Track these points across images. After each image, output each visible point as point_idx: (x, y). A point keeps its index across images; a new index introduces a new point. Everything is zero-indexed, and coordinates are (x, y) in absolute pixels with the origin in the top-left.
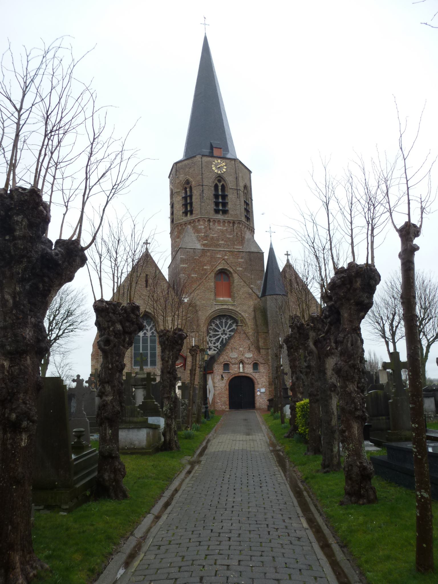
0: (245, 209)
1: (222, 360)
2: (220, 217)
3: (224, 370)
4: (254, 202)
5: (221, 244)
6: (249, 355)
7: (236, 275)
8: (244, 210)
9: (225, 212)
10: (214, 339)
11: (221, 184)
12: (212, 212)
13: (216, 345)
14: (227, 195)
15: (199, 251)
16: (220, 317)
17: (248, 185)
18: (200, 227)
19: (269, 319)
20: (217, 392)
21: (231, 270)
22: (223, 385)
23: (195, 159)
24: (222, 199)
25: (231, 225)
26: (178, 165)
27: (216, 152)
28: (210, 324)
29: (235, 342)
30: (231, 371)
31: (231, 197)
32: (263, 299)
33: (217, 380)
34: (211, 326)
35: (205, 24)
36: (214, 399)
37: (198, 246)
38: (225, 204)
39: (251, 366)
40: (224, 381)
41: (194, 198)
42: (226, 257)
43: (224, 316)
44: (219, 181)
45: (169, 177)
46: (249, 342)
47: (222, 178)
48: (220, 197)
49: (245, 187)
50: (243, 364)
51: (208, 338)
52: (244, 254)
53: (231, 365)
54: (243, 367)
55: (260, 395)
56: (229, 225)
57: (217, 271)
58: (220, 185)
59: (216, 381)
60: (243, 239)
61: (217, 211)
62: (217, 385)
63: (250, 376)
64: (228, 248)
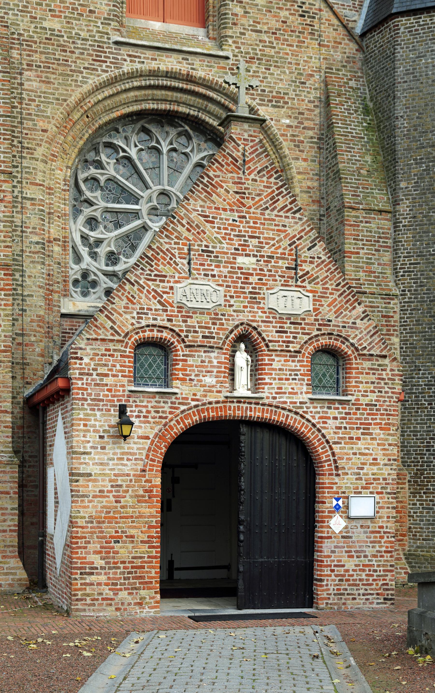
1: (127, 321)
6: (292, 301)
10: (109, 236)
13: (119, 268)
19: (401, 144)
20: (90, 509)
22: (130, 467)
30: (178, 388)
33: (92, 437)
34: (99, 165)
39: (300, 365)
50: (253, 350)
51: (77, 228)
53: (181, 351)
54: (256, 371)
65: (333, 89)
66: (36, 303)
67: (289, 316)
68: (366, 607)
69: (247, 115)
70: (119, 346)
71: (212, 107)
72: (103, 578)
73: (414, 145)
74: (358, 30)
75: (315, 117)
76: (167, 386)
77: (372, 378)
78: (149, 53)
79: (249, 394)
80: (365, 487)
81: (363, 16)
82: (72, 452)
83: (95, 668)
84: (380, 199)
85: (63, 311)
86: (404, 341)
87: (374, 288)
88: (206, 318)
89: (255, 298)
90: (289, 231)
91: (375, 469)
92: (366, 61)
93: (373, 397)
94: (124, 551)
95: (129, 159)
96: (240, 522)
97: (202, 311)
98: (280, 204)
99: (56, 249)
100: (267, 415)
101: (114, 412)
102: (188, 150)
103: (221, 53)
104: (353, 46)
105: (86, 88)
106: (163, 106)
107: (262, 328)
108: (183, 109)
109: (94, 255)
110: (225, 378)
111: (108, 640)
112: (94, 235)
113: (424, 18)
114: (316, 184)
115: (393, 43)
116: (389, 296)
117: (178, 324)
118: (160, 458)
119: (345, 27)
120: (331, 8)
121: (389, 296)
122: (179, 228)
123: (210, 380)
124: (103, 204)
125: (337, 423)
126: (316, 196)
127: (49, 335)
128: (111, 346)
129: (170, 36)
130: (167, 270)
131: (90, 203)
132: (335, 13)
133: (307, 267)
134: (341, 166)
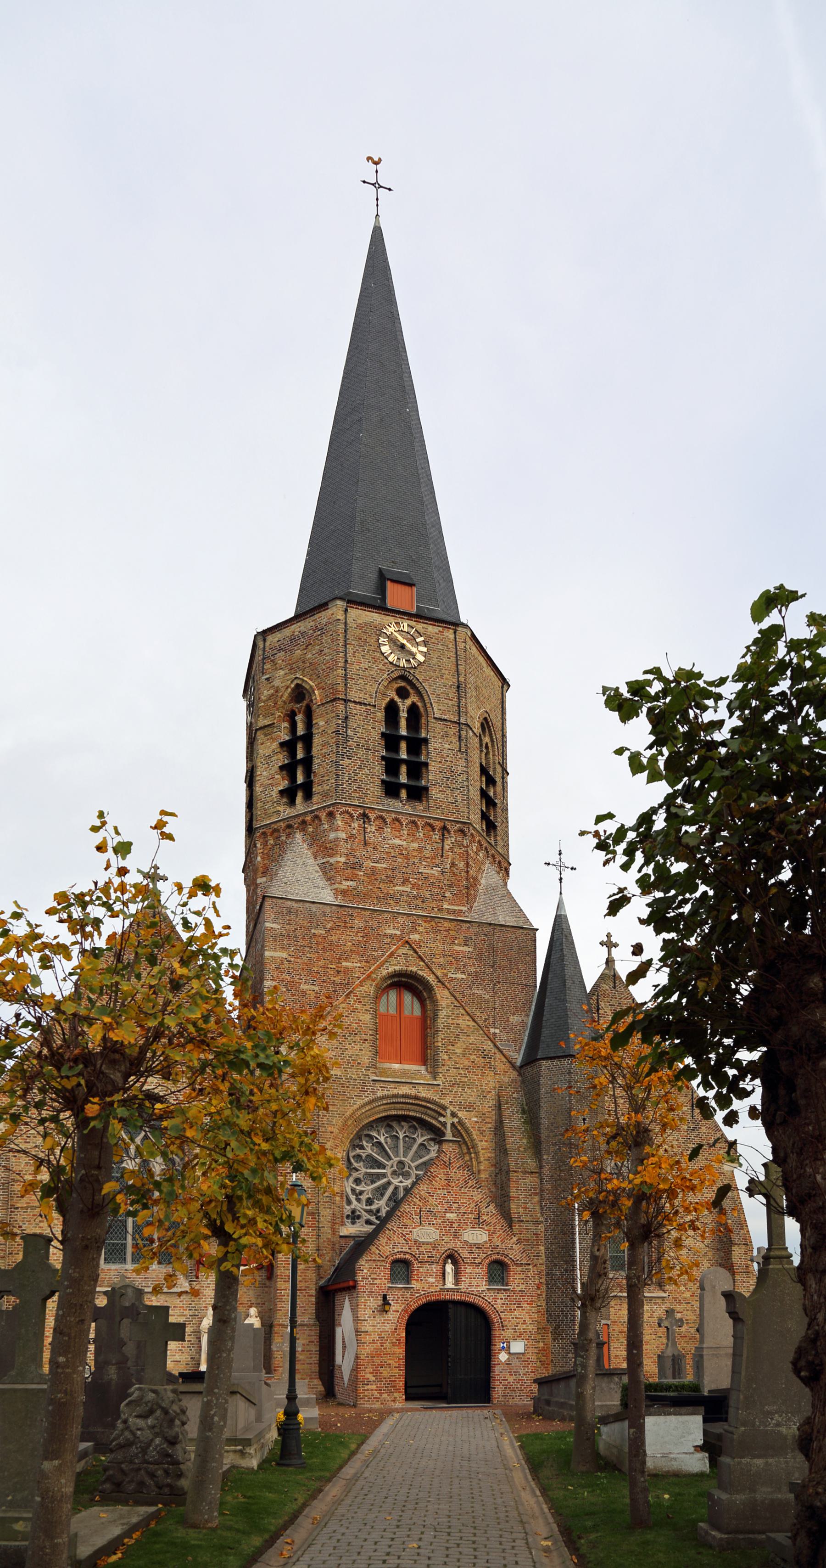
0: (484, 794)
1: (387, 1250)
2: (401, 806)
3: (393, 1278)
4: (511, 781)
5: (402, 894)
6: (477, 1236)
7: (446, 992)
8: (478, 769)
9: (418, 794)
10: (368, 1189)
11: (408, 702)
12: (375, 790)
13: (374, 1207)
14: (426, 741)
15: (328, 909)
16: (388, 1121)
17: (495, 720)
18: (332, 836)
19: (544, 1134)
20: (367, 1350)
21: (431, 979)
22: (388, 1327)
23: (323, 617)
24: (409, 752)
25: (436, 836)
26: (270, 638)
27: (396, 595)
28: (356, 1144)
29: (433, 1193)
30: (415, 1284)
31: (440, 747)
32: (529, 1070)
33: (368, 1312)
35: (377, 185)
36: (355, 1370)
37: (327, 896)
38: (417, 769)
39: (482, 1271)
40: (392, 1316)
41: (317, 741)
42: (415, 937)
43: (401, 1119)
44: (402, 693)
45: (244, 696)
46: (477, 1196)
47: (410, 683)
48: (403, 745)
49: (486, 725)
50: (455, 1263)
51: (349, 1185)
52: (474, 929)
54: (457, 1274)
55: (508, 1363)
56: (430, 837)
57: (385, 979)
58: (403, 706)
59: (365, 1313)
60: (472, 884)
61: (391, 790)
62: (370, 1329)
63: (478, 1301)
64: (422, 909)
65: (503, 1100)
66: (327, 1230)
67: (475, 1244)
68: (521, 1403)
69: (451, 1138)
70: (383, 1264)
71: (429, 1112)
72: (374, 1387)
73: (551, 1134)
74: (518, 1064)
75: (492, 1117)
76: (408, 1283)
77: (523, 1276)
78: (392, 1085)
79: (453, 1287)
80: (519, 1336)
81: (521, 1055)
82: (356, 1320)
83: (380, 1424)
84: (532, 1164)
85: (341, 1234)
86: (547, 1249)
87: (528, 1218)
88: (429, 1247)
89: (456, 1235)
90: (475, 1198)
91: (524, 1326)
92: (523, 1082)
93: (523, 1287)
94: (385, 1372)
95: (380, 1143)
96: (449, 1356)
97: (427, 1243)
98: (470, 1184)
99: (338, 1198)
100: (463, 1298)
101: (380, 1298)
102: (415, 1136)
103: (435, 1083)
104: (515, 1073)
105: (356, 1107)
106: (400, 1113)
107: (461, 1251)
108: (412, 1114)
109: (359, 1200)
110: (440, 1279)
111: (385, 1414)
112: (359, 1188)
113: (555, 1062)
114: (493, 1155)
115: (538, 1075)
116: (537, 1223)
117: (415, 1251)
118: (405, 1322)
119: (510, 1062)
120: (502, 1052)
121: (537, 1223)
122: (415, 1200)
123: (432, 1280)
124: (364, 1170)
125: (503, 1301)
126: (494, 1162)
127: (333, 1249)
128: (379, 1263)
129: (404, 1073)
130: (409, 1222)
131: (357, 1170)
132: (504, 1055)
133: (485, 1218)
134: (508, 1146)
